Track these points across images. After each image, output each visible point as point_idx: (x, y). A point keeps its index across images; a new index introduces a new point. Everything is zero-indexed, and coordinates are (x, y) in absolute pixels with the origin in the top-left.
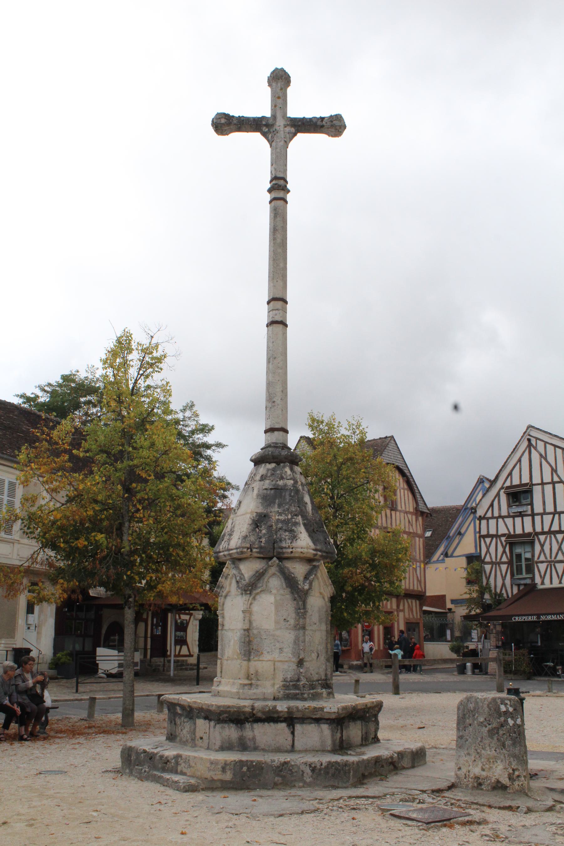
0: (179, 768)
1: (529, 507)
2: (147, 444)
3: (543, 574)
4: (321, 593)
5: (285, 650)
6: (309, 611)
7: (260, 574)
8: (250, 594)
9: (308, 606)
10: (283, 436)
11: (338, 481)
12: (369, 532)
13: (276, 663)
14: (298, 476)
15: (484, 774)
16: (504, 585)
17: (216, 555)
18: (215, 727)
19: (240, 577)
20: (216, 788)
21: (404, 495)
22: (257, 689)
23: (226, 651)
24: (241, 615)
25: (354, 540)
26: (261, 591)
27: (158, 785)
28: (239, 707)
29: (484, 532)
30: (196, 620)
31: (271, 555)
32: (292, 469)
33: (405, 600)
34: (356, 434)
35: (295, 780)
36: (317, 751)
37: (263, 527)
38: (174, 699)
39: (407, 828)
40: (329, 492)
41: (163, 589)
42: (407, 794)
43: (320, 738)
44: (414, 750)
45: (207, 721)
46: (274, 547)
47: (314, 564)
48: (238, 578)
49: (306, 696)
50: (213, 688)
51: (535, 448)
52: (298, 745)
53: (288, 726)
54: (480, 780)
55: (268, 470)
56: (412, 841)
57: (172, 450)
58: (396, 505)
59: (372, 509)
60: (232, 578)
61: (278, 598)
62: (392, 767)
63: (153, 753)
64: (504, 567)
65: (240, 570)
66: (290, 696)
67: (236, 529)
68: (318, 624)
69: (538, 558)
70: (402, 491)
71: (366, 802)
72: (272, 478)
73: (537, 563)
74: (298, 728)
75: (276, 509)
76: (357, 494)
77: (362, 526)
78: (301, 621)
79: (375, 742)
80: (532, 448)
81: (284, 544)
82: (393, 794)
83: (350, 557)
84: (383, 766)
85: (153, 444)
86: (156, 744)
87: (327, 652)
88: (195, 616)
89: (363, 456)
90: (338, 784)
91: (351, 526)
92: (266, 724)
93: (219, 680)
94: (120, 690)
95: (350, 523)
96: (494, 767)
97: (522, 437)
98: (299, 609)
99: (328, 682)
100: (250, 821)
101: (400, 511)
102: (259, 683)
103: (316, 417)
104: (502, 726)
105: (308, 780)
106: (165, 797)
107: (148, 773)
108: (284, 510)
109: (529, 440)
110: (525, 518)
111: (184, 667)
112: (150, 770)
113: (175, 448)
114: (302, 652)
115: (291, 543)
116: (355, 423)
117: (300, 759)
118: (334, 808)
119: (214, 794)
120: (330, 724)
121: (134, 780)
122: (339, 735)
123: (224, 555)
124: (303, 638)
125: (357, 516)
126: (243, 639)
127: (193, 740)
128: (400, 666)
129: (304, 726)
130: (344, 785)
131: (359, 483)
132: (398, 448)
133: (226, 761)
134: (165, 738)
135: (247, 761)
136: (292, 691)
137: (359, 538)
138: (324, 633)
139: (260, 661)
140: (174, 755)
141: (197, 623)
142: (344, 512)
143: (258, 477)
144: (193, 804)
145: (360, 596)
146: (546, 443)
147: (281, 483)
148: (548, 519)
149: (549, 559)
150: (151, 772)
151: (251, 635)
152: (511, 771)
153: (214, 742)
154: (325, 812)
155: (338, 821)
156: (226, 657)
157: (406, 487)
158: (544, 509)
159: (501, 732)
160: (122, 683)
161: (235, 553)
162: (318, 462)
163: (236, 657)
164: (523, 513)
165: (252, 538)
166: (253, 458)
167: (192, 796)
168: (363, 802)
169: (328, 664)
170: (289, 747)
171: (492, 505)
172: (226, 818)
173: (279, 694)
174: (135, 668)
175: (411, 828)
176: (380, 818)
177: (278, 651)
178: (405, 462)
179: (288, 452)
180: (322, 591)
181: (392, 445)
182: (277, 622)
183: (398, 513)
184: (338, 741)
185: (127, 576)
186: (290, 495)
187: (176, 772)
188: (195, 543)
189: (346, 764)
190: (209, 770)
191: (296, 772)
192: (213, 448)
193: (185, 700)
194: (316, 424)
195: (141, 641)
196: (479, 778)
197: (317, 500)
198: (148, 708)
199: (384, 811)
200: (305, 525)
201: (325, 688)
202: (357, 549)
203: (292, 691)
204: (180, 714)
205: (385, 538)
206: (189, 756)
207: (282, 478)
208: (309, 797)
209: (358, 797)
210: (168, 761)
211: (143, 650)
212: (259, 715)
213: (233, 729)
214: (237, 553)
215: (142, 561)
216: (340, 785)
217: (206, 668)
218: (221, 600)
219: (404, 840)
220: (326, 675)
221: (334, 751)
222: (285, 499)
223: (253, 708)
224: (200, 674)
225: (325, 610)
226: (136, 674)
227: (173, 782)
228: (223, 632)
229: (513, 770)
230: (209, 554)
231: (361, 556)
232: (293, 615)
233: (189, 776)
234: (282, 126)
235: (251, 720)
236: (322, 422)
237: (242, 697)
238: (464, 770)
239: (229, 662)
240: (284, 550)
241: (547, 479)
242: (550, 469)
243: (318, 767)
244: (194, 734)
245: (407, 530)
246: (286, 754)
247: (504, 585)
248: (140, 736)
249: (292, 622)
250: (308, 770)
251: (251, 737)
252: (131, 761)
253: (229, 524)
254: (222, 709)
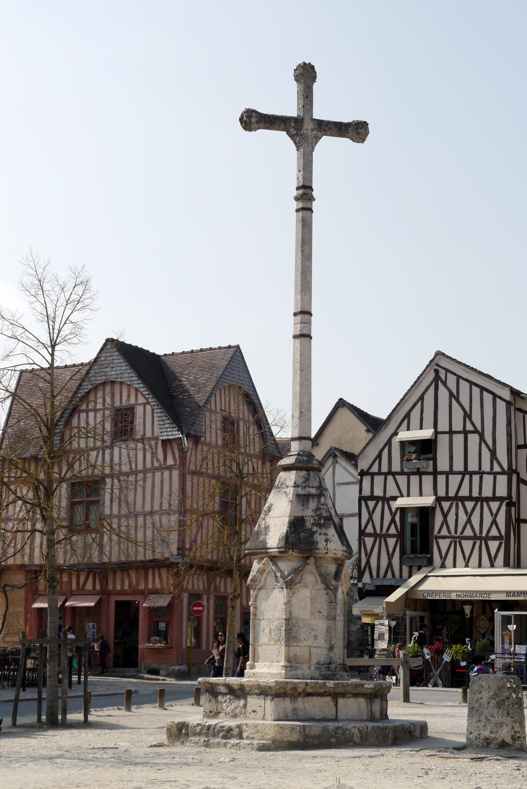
1: (431, 462)
3: (444, 553)
5: (318, 637)
13: (312, 649)
15: (493, 735)
16: (390, 565)
22: (297, 670)
29: (366, 492)
43: (358, 710)
51: (445, 384)
52: (341, 715)
54: (489, 741)
64: (392, 542)
69: (439, 532)
73: (437, 538)
74: (341, 701)
80: (440, 383)
87: (344, 640)
96: (500, 731)
97: (427, 366)
104: (508, 698)
109: (436, 371)
110: (424, 477)
129: (346, 699)
146: (459, 377)
148: (455, 480)
149: (453, 533)
152: (513, 733)
158: (451, 466)
159: (507, 704)
164: (421, 470)
171: (379, 456)
177: (313, 638)
182: (312, 613)
196: (488, 739)
229: (515, 732)
232: (326, 607)
234: (310, 130)
238: (475, 734)
241: (458, 426)
242: (462, 413)
247: (390, 565)
249: (325, 613)
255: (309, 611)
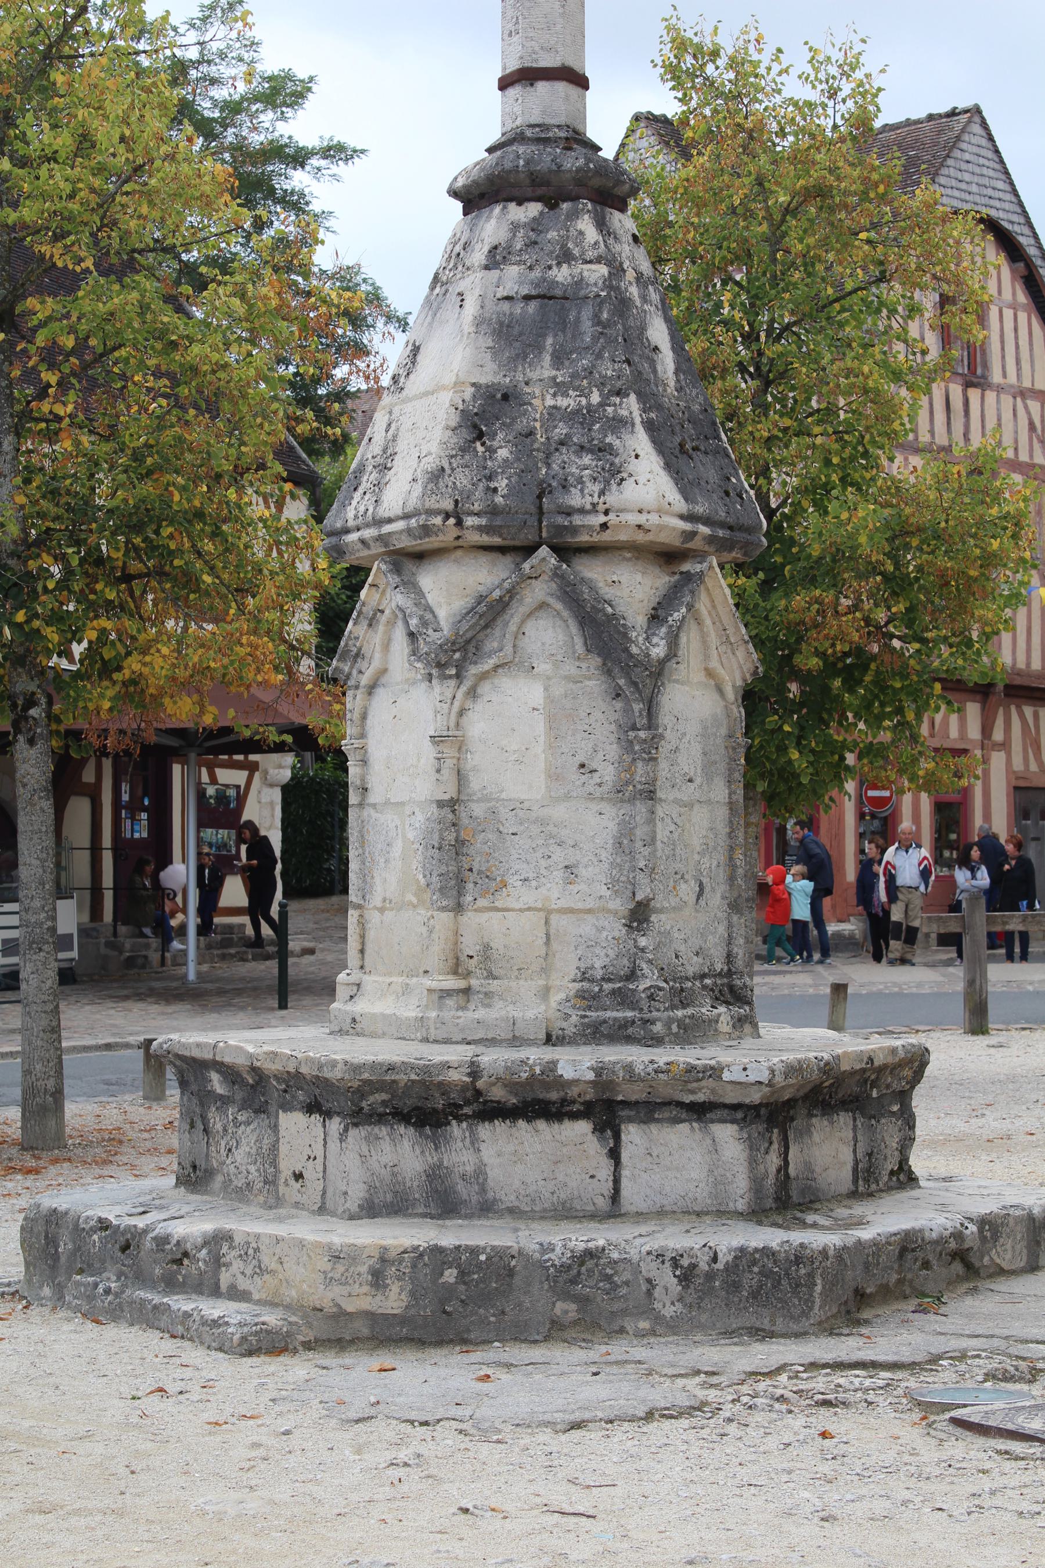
0: (225, 1278)
2: (64, 141)
4: (710, 673)
5: (582, 871)
6: (668, 734)
7: (491, 607)
8: (458, 676)
9: (665, 718)
10: (567, 98)
11: (774, 276)
12: (885, 462)
13: (554, 918)
14: (625, 249)
17: (334, 540)
18: (343, 1137)
19: (421, 618)
20: (352, 1342)
21: (1016, 330)
22: (489, 1006)
23: (378, 880)
24: (429, 751)
25: (827, 487)
26: (497, 667)
27: (153, 1337)
28: (426, 1070)
30: (272, 785)
31: (528, 536)
32: (601, 224)
33: (1013, 708)
34: (841, 95)
35: (625, 1312)
36: (698, 1214)
37: (500, 436)
38: (198, 1045)
39: (1008, 1466)
40: (738, 315)
41: (146, 670)
42: (1010, 1356)
44: (1036, 1211)
45: (316, 1118)
46: (540, 508)
47: (686, 567)
48: (414, 622)
49: (658, 1028)
50: (334, 1005)
53: (599, 1129)
55: (515, 227)
56: (1025, 1506)
57: (158, 163)
58: (985, 366)
59: (897, 376)
60: (391, 623)
61: (558, 690)
62: (958, 1267)
63: (132, 1230)
65: (420, 594)
66: (604, 1029)
67: (401, 446)
68: (698, 780)
70: (1008, 313)
71: (868, 1382)
72: (529, 258)
74: (633, 1135)
75: (545, 369)
76: (841, 325)
77: (861, 440)
78: (640, 769)
79: (901, 1186)
81: (575, 499)
82: (963, 1357)
83: (816, 551)
84: (926, 1265)
85: (85, 142)
86: (141, 1200)
87: (732, 879)
88: (266, 772)
89: (865, 180)
90: (773, 1322)
91: (819, 440)
92: (521, 1123)
93: (352, 979)
94: (13, 1031)
95: (817, 430)
98: (634, 728)
99: (738, 982)
100: (469, 1445)
101: (1000, 389)
102: (494, 985)
103: (689, 34)
105: (669, 1311)
106: (180, 1373)
107: (117, 1295)
108: (574, 376)
111: (232, 951)
112: (124, 1286)
113: (171, 157)
114: (642, 879)
115: (602, 493)
116: (837, 56)
117: (638, 1241)
118: (759, 1401)
119: (348, 1359)
120: (742, 1123)
121: (69, 1320)
122: (773, 1160)
123: (363, 541)
124: (646, 829)
125: (842, 402)
126: (436, 836)
127: (271, 1182)
128: (990, 935)
129: (654, 1128)
130: (795, 1327)
131: (849, 286)
132: (997, 151)
133: (385, 1249)
134: (172, 1180)
135: (458, 1248)
136: (609, 1014)
137: (845, 481)
138: (722, 813)
139: (497, 909)
140: (204, 1234)
141: (277, 795)
142: (793, 388)
143: (478, 256)
144: (274, 1394)
145: (852, 691)
147: (562, 274)
150: (128, 1292)
151: (465, 821)
153: (344, 1188)
154: (728, 1414)
155: (772, 1443)
156: (376, 900)
157: (1022, 298)
160: (18, 1008)
161: (401, 532)
162: (700, 205)
163: (415, 900)
165: (463, 479)
166: (460, 183)
167: (272, 1369)
168: (857, 1381)
169: (735, 918)
170: (603, 1204)
172: (390, 1435)
173: (564, 1025)
174: (61, 955)
175: (1022, 1464)
176: (918, 1431)
177: (559, 875)
178: (1021, 204)
179: (588, 160)
180: (714, 664)
181: (975, 140)
182: (554, 776)
183: (991, 396)
184: (771, 1180)
185: (15, 626)
186: (597, 321)
187: (216, 1292)
188: (258, 509)
189: (799, 1257)
190: (329, 1281)
191: (627, 1283)
192: (315, 162)
193: (237, 1048)
194: (689, 60)
195: (81, 862)
197: (695, 346)
198: (113, 1086)
199: (928, 1409)
200: (650, 427)
201: (727, 1003)
202: (841, 524)
203: (609, 1014)
204: (221, 1097)
205: (942, 481)
206: (258, 1236)
207: (566, 257)
208: (673, 1366)
209: (839, 1366)
210: (186, 1254)
211: (87, 894)
212: (498, 1093)
213: (406, 1144)
214: (409, 531)
215: (68, 573)
216: (780, 1326)
217: (311, 951)
218: (354, 702)
219: (998, 1501)
220: (729, 957)
221: (757, 1214)
222: (577, 334)
223: (475, 1071)
224: (291, 971)
225: (723, 731)
226: (67, 977)
227: (204, 1322)
228: (368, 812)
230: (310, 546)
231: (854, 548)
232: (613, 750)
233: (258, 1302)
235: (467, 1110)
236: (715, 54)
237: (433, 1034)
239: (389, 915)
240: (577, 520)
243: (703, 1266)
244: (274, 1164)
245: (1024, 457)
246: (593, 1225)
248: (89, 1180)
249: (608, 773)
250: (667, 1279)
251: (469, 1169)
252: (56, 1257)
253: (377, 429)
254: (366, 1076)
255: (542, 765)
